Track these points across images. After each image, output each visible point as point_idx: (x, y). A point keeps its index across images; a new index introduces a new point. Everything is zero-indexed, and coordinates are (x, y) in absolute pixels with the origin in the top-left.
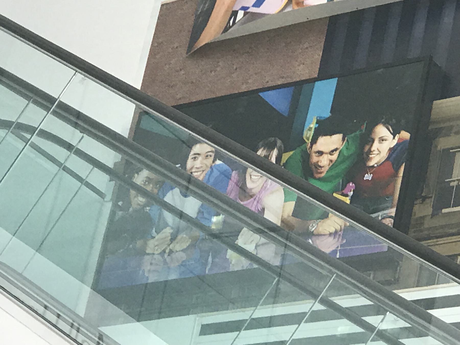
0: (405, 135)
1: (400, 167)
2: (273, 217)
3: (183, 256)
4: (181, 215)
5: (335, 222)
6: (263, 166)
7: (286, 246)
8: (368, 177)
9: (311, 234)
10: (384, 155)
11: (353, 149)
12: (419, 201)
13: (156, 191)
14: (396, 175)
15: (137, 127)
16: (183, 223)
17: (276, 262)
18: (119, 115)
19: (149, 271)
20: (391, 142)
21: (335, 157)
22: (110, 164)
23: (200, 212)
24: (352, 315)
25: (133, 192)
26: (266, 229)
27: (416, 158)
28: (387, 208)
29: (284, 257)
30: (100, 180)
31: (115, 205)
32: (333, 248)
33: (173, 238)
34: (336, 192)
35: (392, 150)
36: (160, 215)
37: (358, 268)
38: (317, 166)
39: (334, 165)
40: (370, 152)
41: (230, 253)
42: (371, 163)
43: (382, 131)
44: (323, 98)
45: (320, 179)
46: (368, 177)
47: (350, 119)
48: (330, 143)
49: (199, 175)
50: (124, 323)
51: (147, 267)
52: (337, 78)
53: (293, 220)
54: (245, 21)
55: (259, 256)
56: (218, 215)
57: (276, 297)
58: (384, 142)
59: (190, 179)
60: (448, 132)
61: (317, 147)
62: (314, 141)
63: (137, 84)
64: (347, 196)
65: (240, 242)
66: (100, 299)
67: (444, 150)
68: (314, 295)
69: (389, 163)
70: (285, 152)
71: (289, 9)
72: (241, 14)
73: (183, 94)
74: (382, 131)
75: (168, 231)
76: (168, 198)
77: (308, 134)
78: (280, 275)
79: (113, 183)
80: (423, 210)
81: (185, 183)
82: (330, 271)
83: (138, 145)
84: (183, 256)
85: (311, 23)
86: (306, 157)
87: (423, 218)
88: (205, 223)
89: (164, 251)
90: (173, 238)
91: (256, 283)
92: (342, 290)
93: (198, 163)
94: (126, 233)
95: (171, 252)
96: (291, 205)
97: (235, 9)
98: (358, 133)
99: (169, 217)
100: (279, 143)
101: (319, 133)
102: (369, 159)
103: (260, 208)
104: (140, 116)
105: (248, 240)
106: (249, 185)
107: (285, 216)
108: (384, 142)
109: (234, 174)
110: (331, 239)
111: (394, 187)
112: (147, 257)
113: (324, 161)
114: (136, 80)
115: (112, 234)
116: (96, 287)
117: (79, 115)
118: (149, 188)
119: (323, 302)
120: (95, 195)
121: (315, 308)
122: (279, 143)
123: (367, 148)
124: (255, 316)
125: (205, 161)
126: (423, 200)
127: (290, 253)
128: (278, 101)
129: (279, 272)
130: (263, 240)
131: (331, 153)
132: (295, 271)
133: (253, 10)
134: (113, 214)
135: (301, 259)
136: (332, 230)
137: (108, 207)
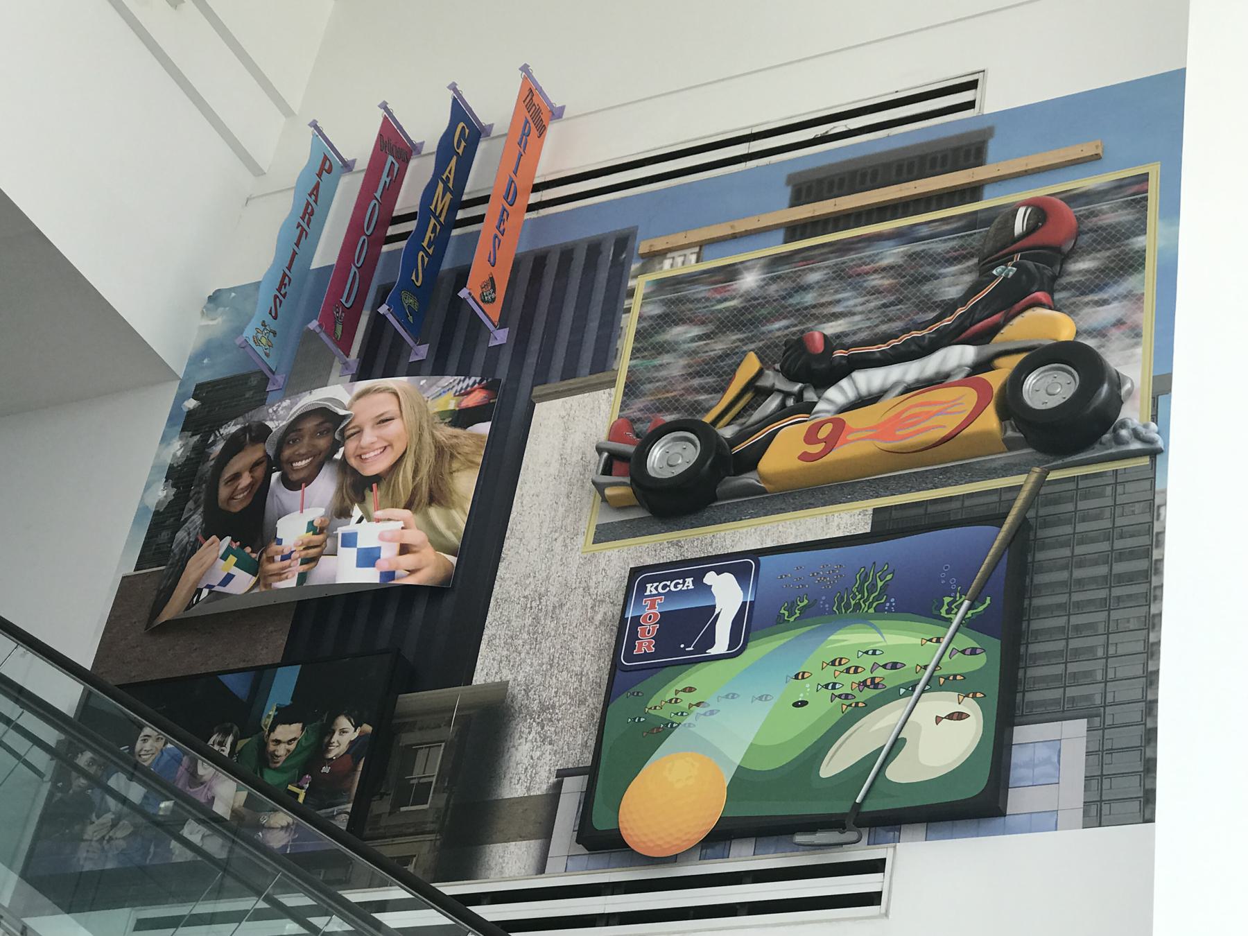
0: (368, 728)
1: (358, 763)
2: (221, 809)
3: (123, 844)
4: (124, 800)
5: (282, 818)
6: (216, 759)
7: (233, 841)
8: (326, 769)
9: (261, 827)
10: (344, 747)
11: (312, 739)
12: (378, 797)
13: (99, 773)
14: (355, 770)
15: (85, 704)
16: (126, 810)
17: (222, 854)
18: (65, 694)
19: (86, 859)
20: (352, 735)
21: (292, 747)
22: (52, 743)
23: (145, 797)
24: (297, 915)
25: (74, 774)
26: (211, 820)
27: (379, 753)
28: (343, 803)
29: (231, 851)
30: (40, 758)
31: (54, 785)
32: (283, 843)
33: (114, 825)
34: (291, 783)
35: (352, 743)
36: (103, 799)
37: (304, 867)
38: (273, 755)
39: (291, 755)
40: (329, 744)
41: (174, 844)
42: (330, 756)
43: (343, 722)
44: (284, 685)
45: (276, 769)
46: (326, 769)
47: (312, 709)
48: (289, 732)
49: (147, 761)
50: (53, 914)
51: (82, 854)
52: (299, 667)
53: (244, 811)
54: (207, 600)
55: (205, 847)
56: (168, 799)
57: (219, 893)
58: (346, 733)
59: (136, 766)
60: (410, 727)
61: (274, 736)
62: (272, 729)
63: (87, 664)
64: (302, 788)
65: (185, 832)
66: (28, 888)
67: (407, 746)
68: (258, 893)
69: (349, 756)
70: (242, 738)
71: (256, 591)
72: (205, 592)
73: (136, 674)
74: (343, 722)
75: (108, 817)
76: (113, 782)
77: (267, 721)
78: (225, 870)
79: (54, 763)
80: (380, 807)
81: (130, 769)
82: (276, 869)
83: (83, 727)
84: (123, 844)
85: (277, 606)
86: (263, 745)
87: (380, 816)
88: (151, 810)
89: (103, 838)
90: (114, 825)
91: (201, 877)
92: (287, 889)
93: (148, 746)
94: (63, 816)
95: (111, 839)
96: (243, 795)
97: (200, 586)
98: (318, 723)
99: (111, 802)
100: (236, 728)
101: (277, 721)
102: (329, 752)
103: (210, 795)
104: (86, 698)
105: (194, 832)
106: (201, 771)
107: (236, 806)
108: (346, 733)
109: (185, 759)
110: (282, 833)
111: (352, 782)
112: (83, 844)
113: (282, 750)
114: (86, 660)
115: (48, 817)
116: (24, 875)
117: (21, 690)
118: (92, 770)
119: (268, 899)
120: (31, 773)
121: (258, 906)
122: (236, 728)
123: (326, 740)
124: (194, 912)
125: (156, 744)
126: (381, 798)
127: (237, 850)
128: (238, 685)
129: (224, 866)
130: (209, 832)
131: (289, 742)
132: (241, 866)
133: (217, 589)
134: (51, 794)
135: (244, 854)
136: (284, 823)
137: (46, 788)
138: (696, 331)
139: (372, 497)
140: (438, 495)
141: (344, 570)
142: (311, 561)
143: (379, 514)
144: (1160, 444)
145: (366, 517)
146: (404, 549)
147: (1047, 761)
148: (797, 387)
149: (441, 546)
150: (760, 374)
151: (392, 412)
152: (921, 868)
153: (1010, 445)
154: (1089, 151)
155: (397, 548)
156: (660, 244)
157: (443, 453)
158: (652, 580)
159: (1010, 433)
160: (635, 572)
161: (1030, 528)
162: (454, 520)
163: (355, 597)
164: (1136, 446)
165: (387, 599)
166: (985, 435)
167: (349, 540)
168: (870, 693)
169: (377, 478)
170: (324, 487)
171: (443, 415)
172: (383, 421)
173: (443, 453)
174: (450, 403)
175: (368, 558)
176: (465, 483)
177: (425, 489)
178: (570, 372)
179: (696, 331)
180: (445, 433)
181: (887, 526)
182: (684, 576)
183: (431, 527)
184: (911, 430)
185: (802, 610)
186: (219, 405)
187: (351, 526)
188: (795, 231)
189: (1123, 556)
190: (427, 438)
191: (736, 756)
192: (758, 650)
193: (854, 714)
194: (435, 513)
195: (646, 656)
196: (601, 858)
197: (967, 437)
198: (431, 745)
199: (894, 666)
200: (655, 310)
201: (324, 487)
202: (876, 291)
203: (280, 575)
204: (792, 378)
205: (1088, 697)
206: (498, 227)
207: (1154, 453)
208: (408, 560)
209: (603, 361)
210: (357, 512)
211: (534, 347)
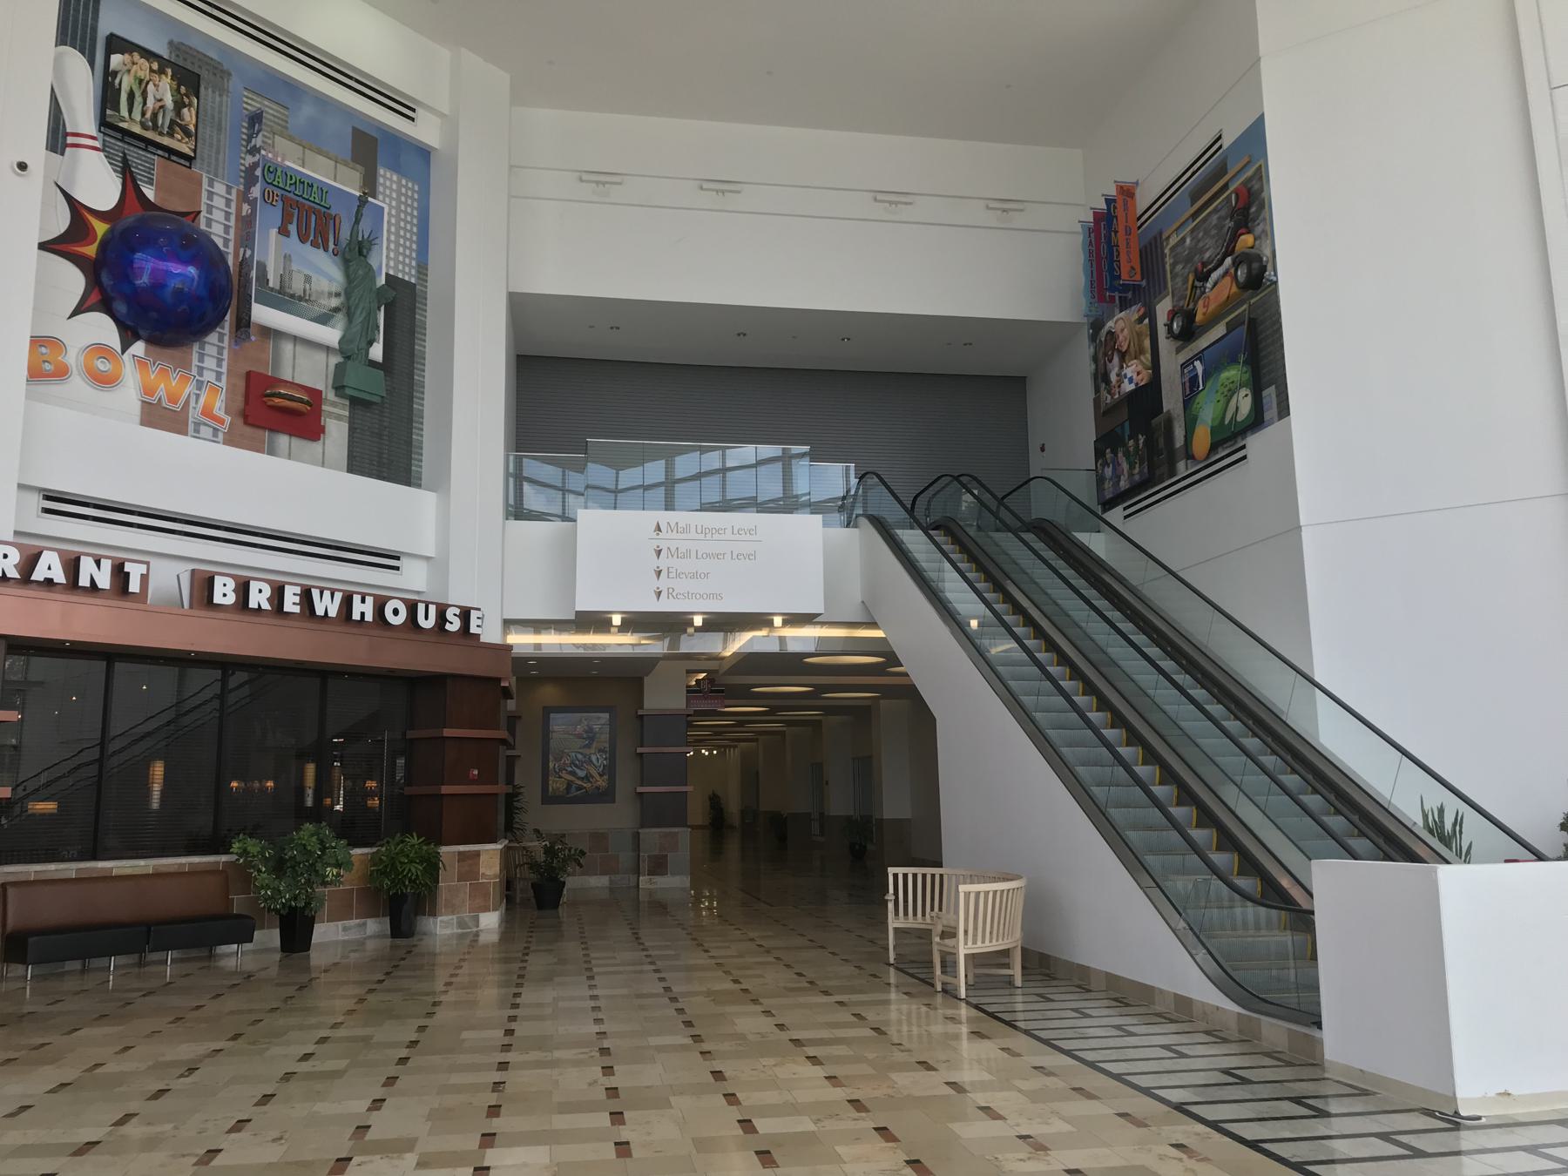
48: (1131, 443)
58: (1142, 439)
140: (1141, 351)
141: (1128, 387)
152: (1255, 444)
154: (1246, 159)
157: (1139, 335)
162: (1147, 358)
163: (1132, 392)
165: (1139, 390)
170: (1116, 359)
173: (1139, 335)
176: (1147, 343)
181: (1231, 328)
184: (825, 1034)
186: (1096, 326)
188: (1195, 215)
192: (1209, 384)
201: (1116, 359)
207: (1276, 283)
209: (1166, 287)
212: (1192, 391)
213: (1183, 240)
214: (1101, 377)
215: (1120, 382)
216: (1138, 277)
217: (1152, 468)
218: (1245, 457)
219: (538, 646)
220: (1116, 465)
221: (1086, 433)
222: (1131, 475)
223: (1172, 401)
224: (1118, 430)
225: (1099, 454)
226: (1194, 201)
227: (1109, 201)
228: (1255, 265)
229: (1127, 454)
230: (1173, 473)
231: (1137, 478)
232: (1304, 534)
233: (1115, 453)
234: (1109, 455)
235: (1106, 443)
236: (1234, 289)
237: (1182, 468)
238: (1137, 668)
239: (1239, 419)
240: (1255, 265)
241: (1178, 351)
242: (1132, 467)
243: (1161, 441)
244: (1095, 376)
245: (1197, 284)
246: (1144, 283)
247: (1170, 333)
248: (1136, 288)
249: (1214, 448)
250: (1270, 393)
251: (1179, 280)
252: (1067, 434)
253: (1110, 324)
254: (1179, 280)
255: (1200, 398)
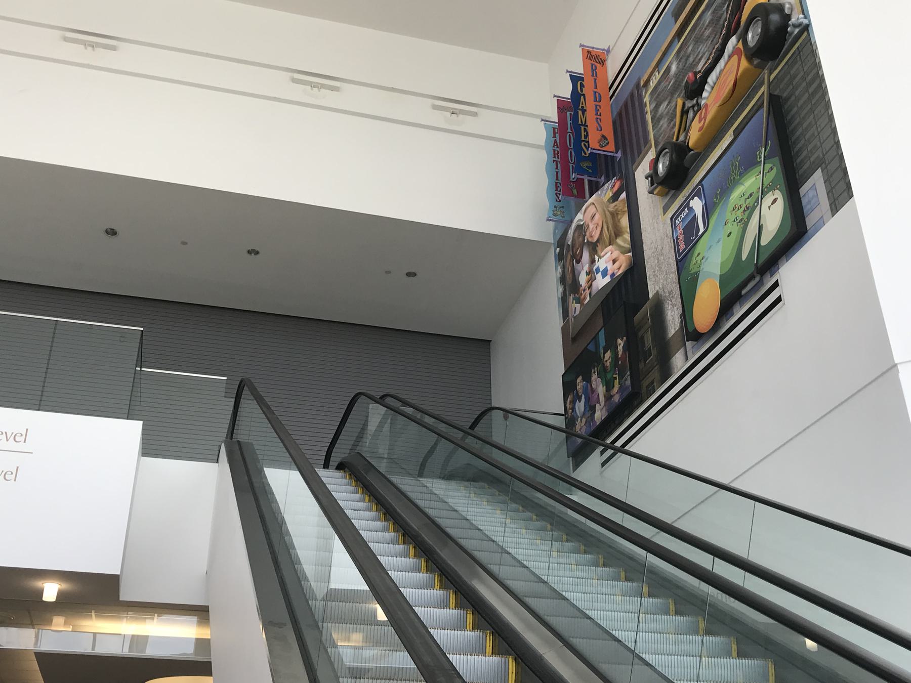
48: (608, 354)
74: (619, 341)
101: (605, 353)
138: (666, 103)
139: (599, 249)
140: (618, 233)
141: (601, 282)
142: (591, 286)
143: (602, 254)
144: (806, 22)
145: (600, 257)
146: (614, 261)
147: (813, 196)
148: (695, 101)
149: (624, 252)
150: (684, 104)
151: (592, 213)
152: (792, 274)
153: (761, 67)
155: (611, 262)
156: (645, 78)
158: (676, 219)
159: (755, 62)
160: (672, 219)
161: (778, 97)
164: (797, 30)
166: (746, 71)
167: (598, 270)
168: (747, 213)
169: (598, 241)
171: (609, 201)
172: (593, 217)
173: (614, 215)
174: (610, 194)
175: (605, 273)
176: (625, 221)
177: (613, 234)
178: (639, 153)
179: (666, 103)
180: (612, 207)
182: (684, 209)
183: (620, 247)
185: (720, 194)
187: (597, 264)
189: (809, 85)
190: (607, 213)
191: (718, 272)
193: (745, 224)
194: (619, 241)
195: (684, 250)
196: (701, 341)
197: (741, 76)
198: (646, 332)
199: (751, 195)
200: (653, 105)
202: (708, 37)
203: (585, 298)
204: (692, 99)
205: (818, 157)
206: (597, 114)
208: (617, 264)
210: (597, 258)
211: (628, 150)
212: (687, 241)
213: (668, 69)
214: (570, 285)
215: (591, 280)
216: (611, 147)
217: (636, 379)
218: (779, 300)
219: (138, 641)
220: (590, 393)
221: (555, 365)
222: (608, 398)
223: (660, 279)
224: (591, 347)
225: (569, 387)
226: (676, 16)
227: (575, 79)
228: (775, 18)
229: (603, 374)
230: (666, 373)
231: (617, 399)
232: (901, 376)
233: (587, 379)
234: (580, 384)
235: (579, 367)
236: (744, 63)
237: (679, 362)
238: (619, 129)
239: (764, 242)
240: (775, 18)
241: (665, 209)
242: (609, 386)
243: (649, 341)
244: (563, 280)
245: (689, 104)
246: (619, 155)
247: (653, 177)
248: (609, 160)
249: (726, 309)
250: (815, 187)
251: (664, 123)
252: (534, 376)
253: (580, 216)
254: (664, 123)
255: (701, 247)
